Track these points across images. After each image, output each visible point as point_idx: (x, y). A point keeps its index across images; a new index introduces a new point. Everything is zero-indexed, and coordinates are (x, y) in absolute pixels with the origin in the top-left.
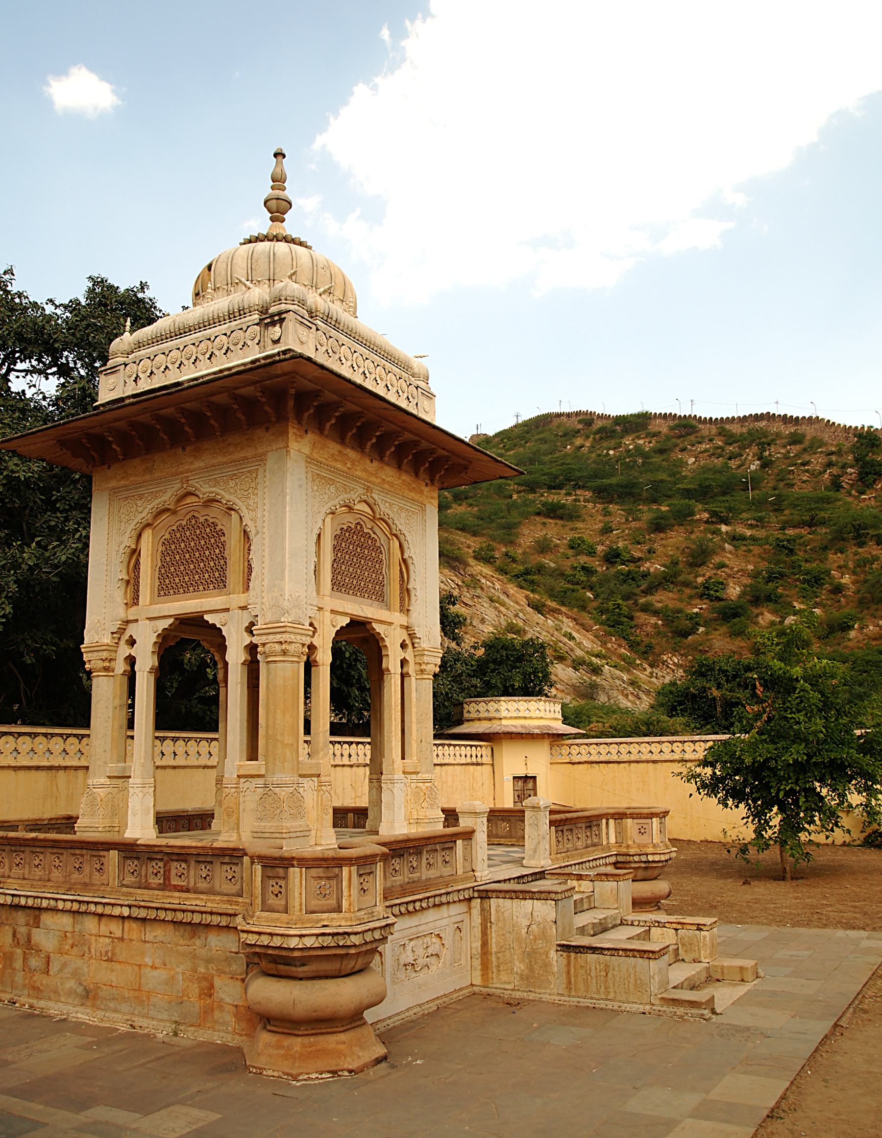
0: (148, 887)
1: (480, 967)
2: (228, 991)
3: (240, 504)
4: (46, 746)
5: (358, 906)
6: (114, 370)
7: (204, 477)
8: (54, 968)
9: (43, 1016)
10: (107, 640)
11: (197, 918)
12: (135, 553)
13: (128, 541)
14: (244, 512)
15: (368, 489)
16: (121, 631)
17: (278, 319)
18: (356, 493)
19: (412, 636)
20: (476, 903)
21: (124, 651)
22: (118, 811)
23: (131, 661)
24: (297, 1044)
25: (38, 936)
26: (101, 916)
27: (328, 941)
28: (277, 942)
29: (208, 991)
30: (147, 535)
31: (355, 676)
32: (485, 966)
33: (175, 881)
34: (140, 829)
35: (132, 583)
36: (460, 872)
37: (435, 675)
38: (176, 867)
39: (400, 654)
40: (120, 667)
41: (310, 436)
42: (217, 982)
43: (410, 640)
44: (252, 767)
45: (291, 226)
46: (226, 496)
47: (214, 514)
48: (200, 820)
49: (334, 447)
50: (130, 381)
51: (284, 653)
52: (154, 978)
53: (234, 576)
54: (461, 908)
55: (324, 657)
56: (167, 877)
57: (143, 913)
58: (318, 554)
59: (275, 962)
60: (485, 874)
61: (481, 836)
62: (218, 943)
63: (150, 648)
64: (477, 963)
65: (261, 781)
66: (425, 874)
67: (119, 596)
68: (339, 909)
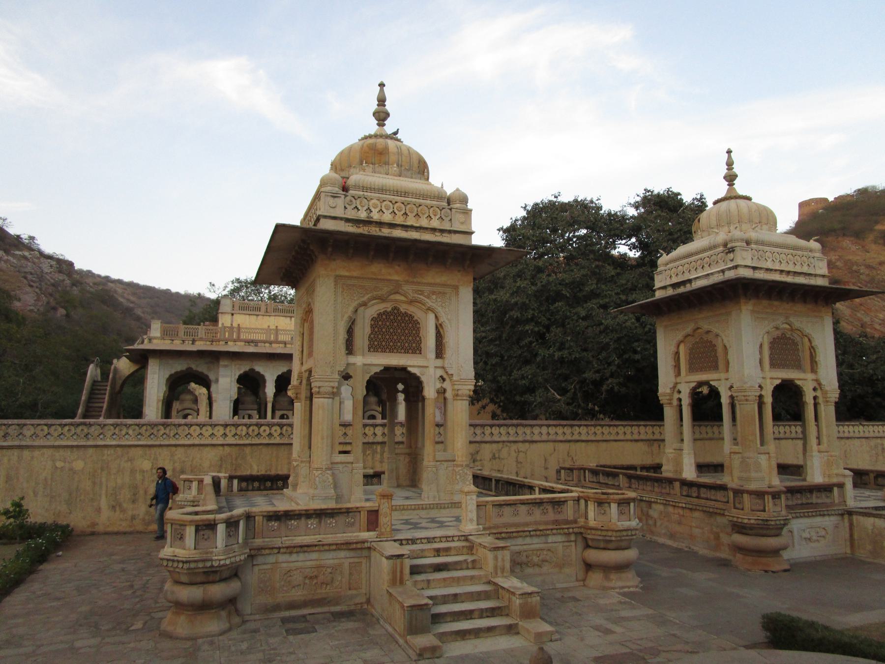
0: (691, 497)
1: (290, 387)
2: (725, 539)
3: (721, 334)
4: (644, 430)
5: (774, 510)
6: (661, 273)
7: (706, 321)
8: (658, 524)
9: (656, 542)
10: (668, 391)
11: (711, 510)
12: (677, 353)
13: (673, 349)
14: (724, 338)
15: (787, 318)
16: (674, 387)
17: (732, 250)
18: (780, 322)
19: (820, 384)
20: (846, 517)
21: (676, 396)
22: (678, 464)
23: (680, 400)
24: (750, 559)
25: (651, 512)
26: (674, 506)
27: (760, 522)
28: (740, 520)
29: (717, 538)
30: (682, 347)
31: (788, 403)
32: (852, 545)
33: (702, 495)
34: (689, 473)
35: (677, 367)
36: (837, 501)
37: (836, 403)
38: (703, 490)
39: (813, 394)
40: (675, 403)
41: (752, 302)
42: (721, 535)
43: (818, 386)
44: (736, 448)
45: (740, 187)
46: (715, 330)
47: (710, 337)
48: (718, 468)
49: (765, 302)
50: (668, 278)
51: (747, 400)
52: (696, 531)
53: (721, 365)
54: (839, 518)
55: (768, 400)
56: (699, 493)
57: (690, 507)
58: (761, 353)
59: (740, 528)
60: (851, 503)
61: (849, 485)
62: (719, 519)
63: (687, 395)
64: (848, 543)
65: (740, 455)
66: (814, 500)
67: (672, 372)
68: (764, 511)
